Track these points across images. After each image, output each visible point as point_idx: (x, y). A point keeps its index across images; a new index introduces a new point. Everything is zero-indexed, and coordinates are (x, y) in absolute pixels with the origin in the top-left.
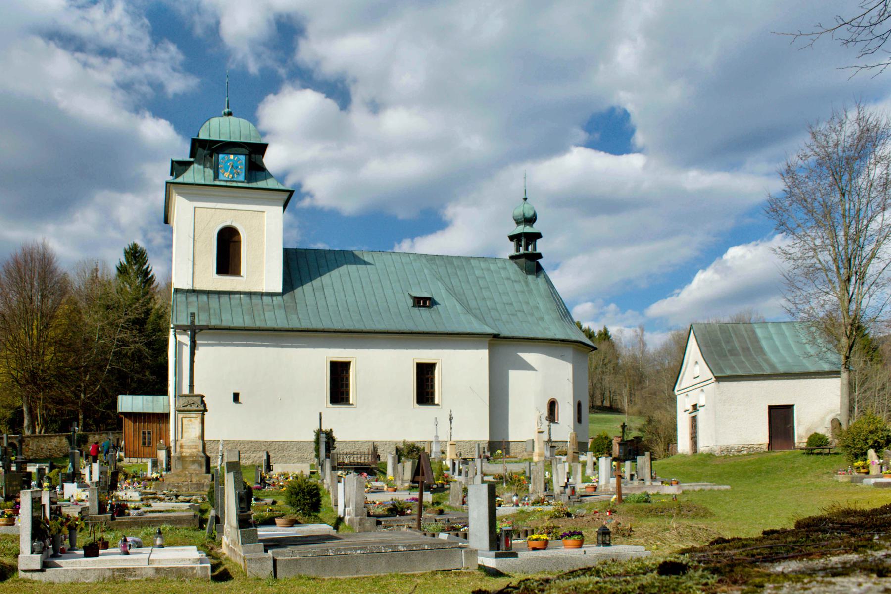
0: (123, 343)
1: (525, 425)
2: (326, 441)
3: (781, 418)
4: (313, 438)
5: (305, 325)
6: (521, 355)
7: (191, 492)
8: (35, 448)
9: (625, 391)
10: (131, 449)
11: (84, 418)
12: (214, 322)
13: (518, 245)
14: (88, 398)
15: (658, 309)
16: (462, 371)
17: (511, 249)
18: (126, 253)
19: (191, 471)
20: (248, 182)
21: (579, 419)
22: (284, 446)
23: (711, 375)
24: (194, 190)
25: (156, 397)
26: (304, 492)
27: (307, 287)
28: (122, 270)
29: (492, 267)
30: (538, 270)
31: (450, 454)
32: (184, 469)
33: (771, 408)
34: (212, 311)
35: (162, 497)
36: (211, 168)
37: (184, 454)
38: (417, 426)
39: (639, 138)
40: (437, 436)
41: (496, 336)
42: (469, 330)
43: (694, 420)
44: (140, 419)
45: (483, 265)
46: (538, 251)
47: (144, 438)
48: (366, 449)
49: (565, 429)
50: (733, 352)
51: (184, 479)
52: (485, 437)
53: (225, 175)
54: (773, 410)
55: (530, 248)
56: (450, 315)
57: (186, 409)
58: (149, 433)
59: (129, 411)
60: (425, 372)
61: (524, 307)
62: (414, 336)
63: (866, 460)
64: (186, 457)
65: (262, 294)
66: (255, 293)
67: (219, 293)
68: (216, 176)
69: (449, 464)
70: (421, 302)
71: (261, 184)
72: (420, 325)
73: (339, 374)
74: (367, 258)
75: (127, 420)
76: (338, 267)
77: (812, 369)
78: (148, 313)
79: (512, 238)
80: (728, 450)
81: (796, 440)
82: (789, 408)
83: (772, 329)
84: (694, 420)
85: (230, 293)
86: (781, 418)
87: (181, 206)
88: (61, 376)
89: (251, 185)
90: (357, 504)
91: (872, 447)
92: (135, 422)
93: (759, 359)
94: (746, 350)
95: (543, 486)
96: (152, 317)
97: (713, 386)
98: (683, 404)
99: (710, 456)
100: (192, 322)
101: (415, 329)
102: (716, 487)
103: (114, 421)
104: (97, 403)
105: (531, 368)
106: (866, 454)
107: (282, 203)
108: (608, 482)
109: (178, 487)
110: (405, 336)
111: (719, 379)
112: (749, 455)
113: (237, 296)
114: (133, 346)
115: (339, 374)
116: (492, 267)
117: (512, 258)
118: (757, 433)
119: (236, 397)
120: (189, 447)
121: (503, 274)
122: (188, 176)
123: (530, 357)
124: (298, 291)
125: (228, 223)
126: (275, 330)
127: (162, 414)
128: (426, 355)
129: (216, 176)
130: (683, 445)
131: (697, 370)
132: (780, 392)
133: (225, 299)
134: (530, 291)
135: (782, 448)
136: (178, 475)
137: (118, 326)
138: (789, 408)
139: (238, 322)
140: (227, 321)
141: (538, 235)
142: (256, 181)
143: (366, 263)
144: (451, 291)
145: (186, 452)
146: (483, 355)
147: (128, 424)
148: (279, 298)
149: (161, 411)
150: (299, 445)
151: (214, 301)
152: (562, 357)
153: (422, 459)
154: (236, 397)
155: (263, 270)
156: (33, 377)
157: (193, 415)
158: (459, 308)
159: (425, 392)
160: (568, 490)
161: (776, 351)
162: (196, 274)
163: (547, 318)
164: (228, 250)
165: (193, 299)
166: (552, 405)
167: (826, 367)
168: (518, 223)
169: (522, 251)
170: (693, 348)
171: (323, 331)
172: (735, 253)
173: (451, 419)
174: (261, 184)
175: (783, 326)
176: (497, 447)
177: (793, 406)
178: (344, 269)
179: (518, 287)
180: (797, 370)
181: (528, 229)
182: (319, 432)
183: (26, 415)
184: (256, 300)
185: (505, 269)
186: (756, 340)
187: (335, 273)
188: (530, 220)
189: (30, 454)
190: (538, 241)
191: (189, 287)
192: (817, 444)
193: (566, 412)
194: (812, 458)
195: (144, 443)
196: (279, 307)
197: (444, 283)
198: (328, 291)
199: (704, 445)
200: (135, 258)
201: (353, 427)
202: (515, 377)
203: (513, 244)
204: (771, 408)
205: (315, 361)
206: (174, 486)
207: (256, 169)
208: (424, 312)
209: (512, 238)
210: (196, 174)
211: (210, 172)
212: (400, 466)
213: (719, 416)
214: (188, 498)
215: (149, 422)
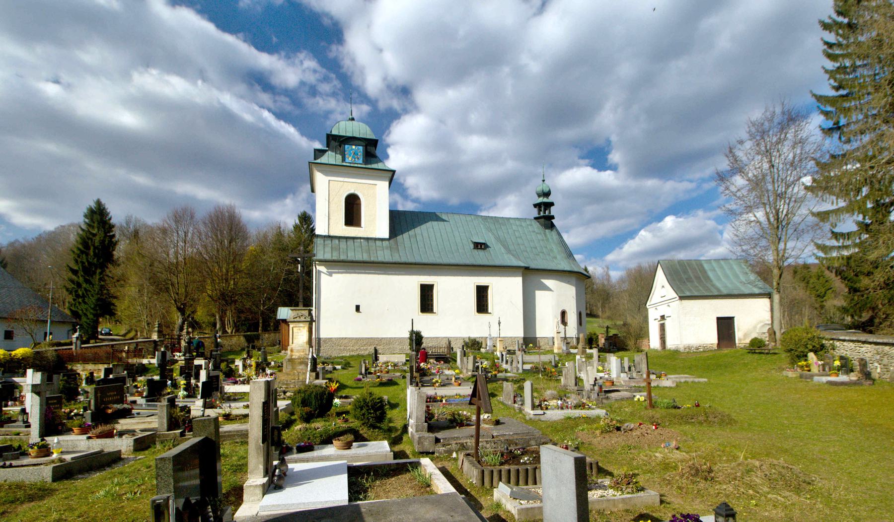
1: (546, 327)
2: (416, 338)
3: (725, 326)
4: (407, 335)
5: (404, 259)
6: (543, 281)
9: (599, 305)
12: (343, 257)
13: (540, 211)
15: (611, 257)
16: (506, 291)
17: (535, 212)
18: (299, 217)
21: (580, 323)
22: (390, 341)
23: (675, 295)
24: (330, 169)
26: (368, 406)
27: (406, 235)
28: (296, 227)
29: (524, 224)
30: (552, 226)
31: (499, 347)
32: (294, 369)
33: (719, 319)
38: (477, 327)
39: (615, 157)
41: (527, 268)
42: (509, 264)
43: (662, 328)
45: (518, 223)
48: (444, 344)
49: (572, 330)
50: (689, 279)
52: (520, 334)
53: (349, 159)
54: (720, 320)
55: (547, 212)
56: (497, 255)
60: (482, 293)
61: (544, 250)
63: (806, 360)
65: (376, 239)
66: (371, 239)
67: (347, 238)
68: (344, 160)
69: (499, 354)
70: (480, 246)
71: (374, 166)
72: (478, 261)
73: (426, 293)
74: (444, 217)
77: (747, 292)
79: (535, 206)
80: (689, 348)
81: (737, 342)
82: (731, 319)
83: (714, 264)
84: (662, 328)
85: (354, 238)
86: (725, 326)
87: (321, 179)
89: (369, 166)
90: (417, 417)
91: (811, 351)
93: (709, 285)
94: (698, 278)
95: (573, 382)
97: (677, 303)
98: (653, 315)
99: (676, 352)
101: (475, 263)
102: (697, 380)
105: (550, 290)
106: (806, 356)
107: (388, 179)
108: (618, 376)
109: (287, 384)
111: (681, 298)
112: (704, 351)
115: (426, 293)
117: (536, 218)
118: (711, 337)
119: (358, 308)
120: (298, 351)
121: (530, 228)
122: (324, 159)
123: (549, 282)
124: (399, 238)
125: (352, 192)
126: (383, 263)
128: (483, 281)
129: (344, 160)
130: (654, 342)
131: (663, 292)
132: (725, 308)
133: (350, 242)
134: (548, 240)
135: (727, 347)
136: (288, 374)
138: (731, 319)
139: (359, 257)
140: (351, 256)
141: (552, 204)
142: (371, 164)
143: (444, 220)
144: (498, 239)
146: (518, 281)
148: (387, 242)
150: (400, 340)
151: (343, 244)
152: (568, 283)
153: (478, 383)
154: (358, 308)
155: (376, 222)
156: (223, 296)
157: (301, 325)
158: (503, 250)
159: (482, 306)
160: (596, 388)
161: (719, 279)
163: (558, 257)
164: (352, 210)
165: (328, 242)
166: (563, 313)
167: (757, 291)
168: (539, 196)
169: (542, 214)
170: (660, 277)
171: (415, 264)
172: (669, 221)
173: (499, 323)
174: (374, 166)
175: (722, 262)
176: (529, 342)
178: (429, 224)
179: (540, 237)
180: (736, 292)
181: (545, 200)
182: (412, 332)
184: (371, 243)
185: (531, 225)
186: (704, 272)
187: (424, 227)
188: (547, 194)
190: (552, 208)
191: (326, 234)
192: (756, 346)
193: (572, 318)
194: (756, 356)
196: (387, 248)
197: (493, 234)
198: (419, 238)
199: (671, 344)
200: (305, 221)
201: (437, 329)
202: (539, 294)
203: (536, 210)
204: (719, 319)
205: (411, 283)
206: (284, 384)
209: (535, 206)
210: (330, 158)
211: (339, 157)
212: (465, 359)
213: (682, 323)
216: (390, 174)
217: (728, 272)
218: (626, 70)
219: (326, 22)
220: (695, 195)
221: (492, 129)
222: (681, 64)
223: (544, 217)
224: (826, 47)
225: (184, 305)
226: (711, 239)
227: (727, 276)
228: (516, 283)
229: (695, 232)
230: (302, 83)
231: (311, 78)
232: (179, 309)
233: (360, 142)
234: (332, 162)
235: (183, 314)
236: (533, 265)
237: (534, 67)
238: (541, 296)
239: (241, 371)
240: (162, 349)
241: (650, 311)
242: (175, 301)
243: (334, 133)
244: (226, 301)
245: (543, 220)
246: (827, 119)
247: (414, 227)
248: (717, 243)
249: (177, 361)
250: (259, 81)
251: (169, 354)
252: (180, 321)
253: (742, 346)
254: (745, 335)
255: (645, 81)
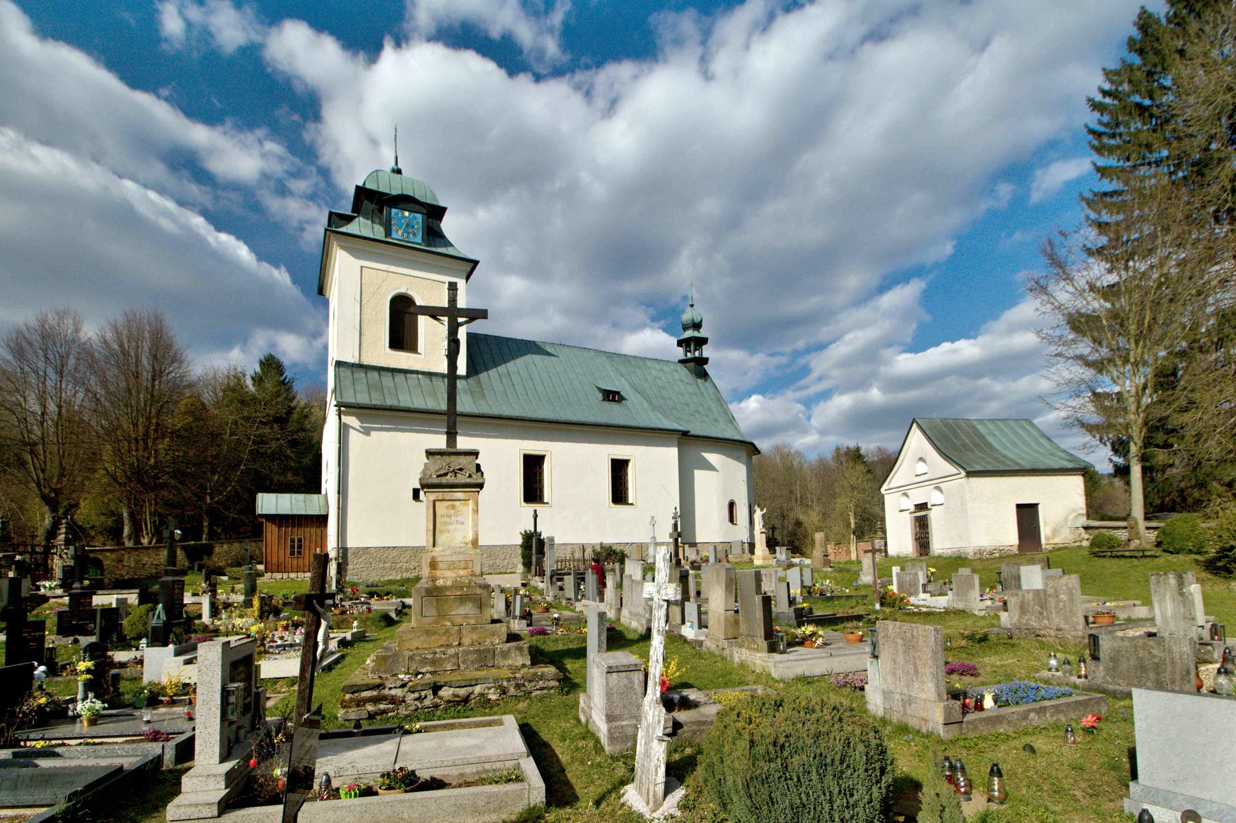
0: (261, 441)
1: (710, 528)
3: (1027, 514)
4: (519, 541)
5: (495, 411)
7: (473, 674)
8: (133, 565)
10: (275, 560)
11: (210, 526)
14: (217, 502)
16: (654, 466)
17: (680, 353)
18: (261, 363)
19: (458, 620)
20: (429, 245)
24: (361, 246)
25: (308, 496)
29: (665, 368)
30: (704, 375)
33: (1019, 506)
34: (386, 390)
35: (398, 692)
36: (381, 224)
37: (440, 582)
40: (654, 538)
41: (685, 434)
44: (287, 522)
45: (657, 366)
46: (705, 355)
47: (292, 547)
51: (443, 640)
53: (397, 235)
56: (637, 412)
57: (444, 480)
58: (300, 540)
59: (273, 512)
60: (619, 468)
62: (610, 430)
64: (445, 588)
68: (388, 233)
70: (611, 396)
72: (608, 419)
75: (269, 524)
76: (505, 362)
77: (1056, 466)
78: (290, 411)
79: (680, 343)
80: (980, 552)
81: (1043, 541)
82: (1033, 507)
85: (405, 372)
86: (1027, 514)
88: (180, 475)
92: (280, 527)
94: (977, 445)
96: (295, 416)
100: (453, 300)
103: (254, 526)
104: (227, 508)
109: (433, 662)
110: (601, 430)
111: (970, 474)
113: (415, 376)
114: (274, 445)
116: (665, 368)
117: (681, 362)
120: (452, 566)
122: (352, 228)
123: (712, 458)
125: (403, 290)
127: (318, 517)
129: (388, 233)
133: (400, 378)
134: (702, 394)
136: (428, 633)
137: (254, 422)
138: (1033, 507)
139: (418, 403)
140: (405, 401)
143: (549, 354)
144: (634, 387)
145: (446, 578)
147: (271, 531)
149: (316, 512)
151: (387, 379)
152: (738, 459)
162: (364, 345)
164: (403, 320)
165: (360, 375)
166: (732, 505)
175: (1001, 424)
177: (1036, 505)
178: (528, 358)
179: (690, 389)
181: (696, 334)
183: (126, 522)
188: (697, 326)
189: (124, 572)
195: (292, 553)
198: (515, 379)
202: (700, 476)
204: (1019, 506)
206: (424, 661)
207: (434, 234)
208: (614, 407)
214: (462, 692)
215: (300, 525)
216: (469, 267)
217: (1014, 438)
218: (710, 206)
219: (298, 87)
220: (788, 371)
221: (535, 269)
222: (777, 206)
223: (694, 360)
224: (1091, 137)
225: (57, 492)
226: (797, 426)
227: (1024, 442)
228: (670, 454)
229: (781, 417)
230: (265, 176)
231: (277, 169)
232: (44, 498)
233: (418, 208)
234: (366, 233)
235: (54, 509)
236: (695, 430)
237: (599, 191)
238: (701, 478)
239: (206, 619)
240: (11, 574)
241: (886, 497)
242: (39, 486)
243: (368, 186)
244: (144, 484)
245: (692, 364)
246: (1100, 234)
247: (514, 357)
248: (805, 431)
249: (45, 599)
250: (187, 165)
251: (26, 583)
252: (48, 521)
253: (1049, 547)
254: (1055, 532)
255: (733, 222)
